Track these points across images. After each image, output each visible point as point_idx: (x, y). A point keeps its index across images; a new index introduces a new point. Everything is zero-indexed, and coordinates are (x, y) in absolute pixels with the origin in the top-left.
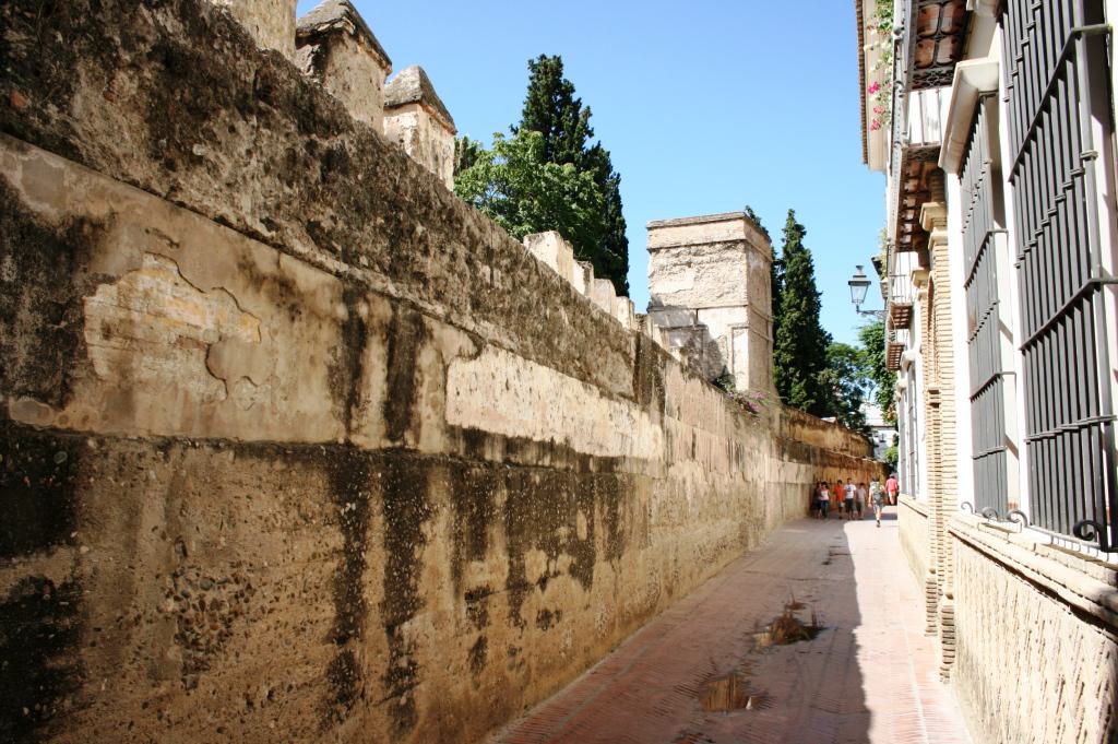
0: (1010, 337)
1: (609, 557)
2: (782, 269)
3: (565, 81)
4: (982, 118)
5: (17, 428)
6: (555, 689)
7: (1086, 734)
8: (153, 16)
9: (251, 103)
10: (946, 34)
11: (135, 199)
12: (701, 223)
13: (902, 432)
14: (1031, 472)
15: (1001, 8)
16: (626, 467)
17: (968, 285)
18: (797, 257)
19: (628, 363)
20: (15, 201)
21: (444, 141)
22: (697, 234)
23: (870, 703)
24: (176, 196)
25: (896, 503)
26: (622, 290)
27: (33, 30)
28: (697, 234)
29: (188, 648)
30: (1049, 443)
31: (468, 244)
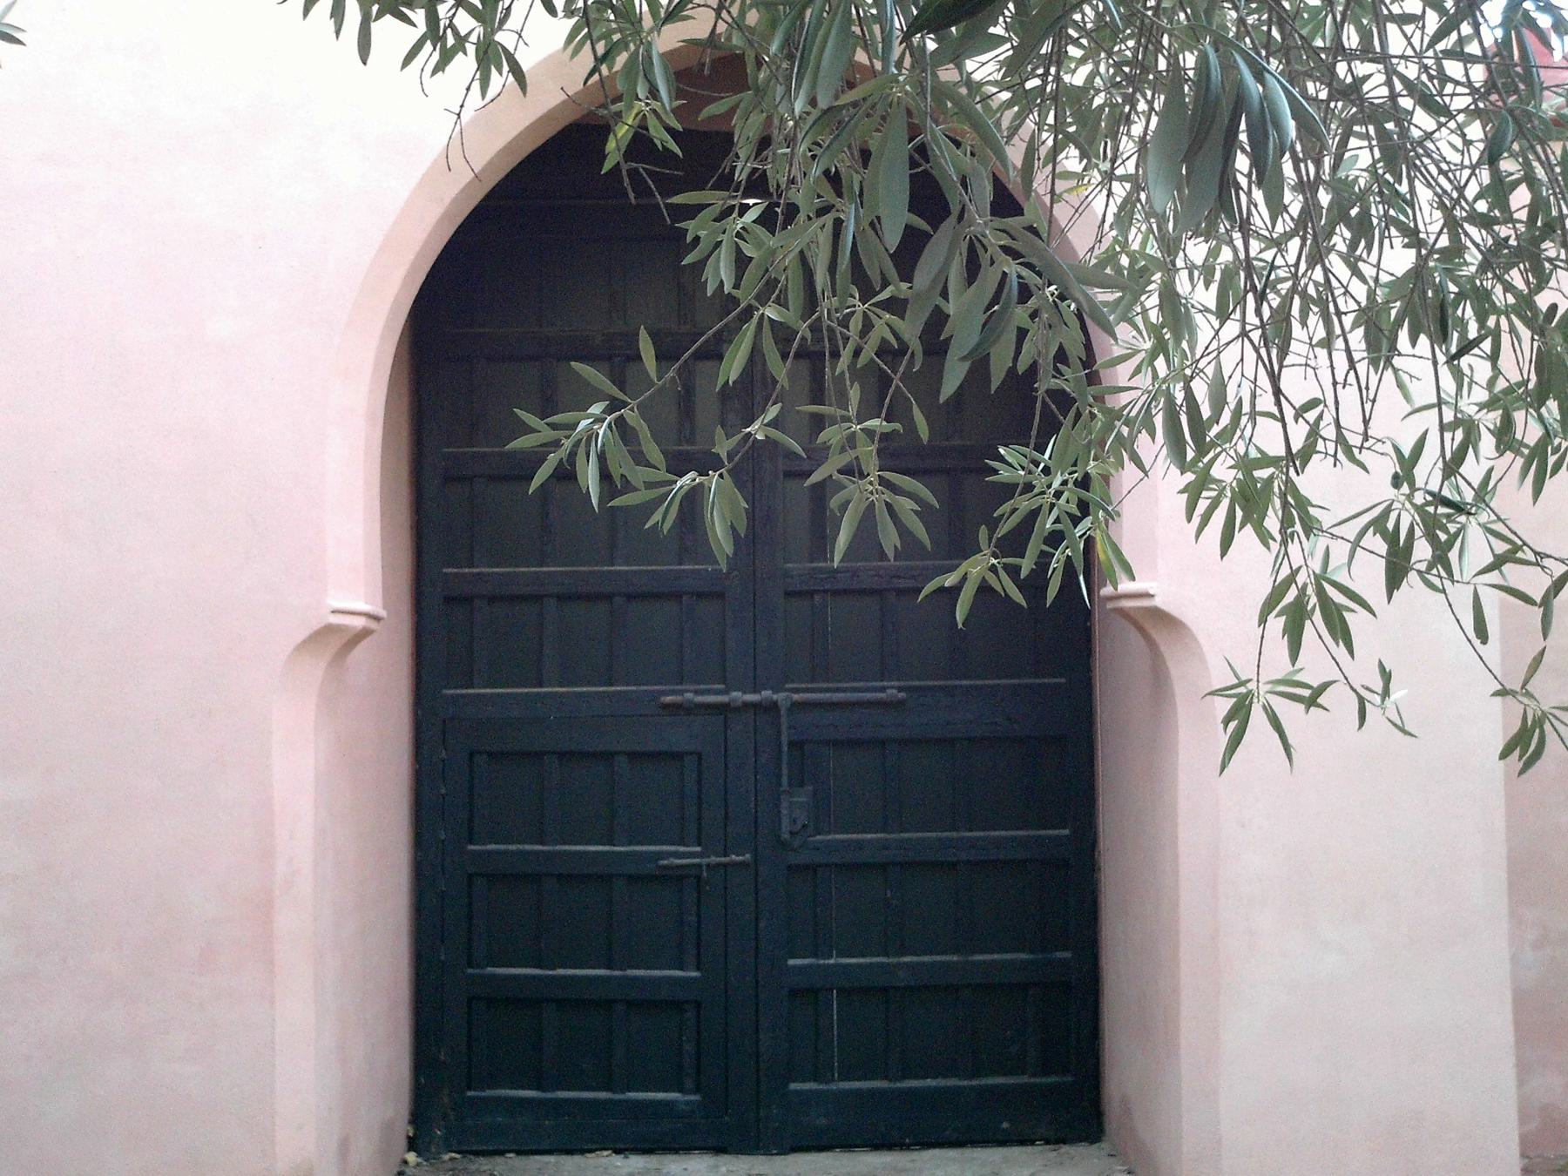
0: (1275, 540)
1: (704, 65)
2: (779, 207)
3: (1419, 137)
4: (671, 8)
5: (1092, 876)
6: (1216, 71)
7: (1367, 689)
8: (1014, 130)
9: (646, 44)
10: (1514, 226)
11: (964, 578)
12: (1399, 712)
13: (866, 109)
14: (1140, 591)
15: (356, 1175)
16: (763, 702)
17: (984, 326)
18: (818, 323)
19: (1278, 518)
20: (877, 533)
21: (819, 346)
22: (1069, 226)
23: (1514, 1070)
24: (1466, 264)
25: (470, 1001)
26: (848, 330)
27: (1297, 301)
28: (1069, 226)
29: (958, 860)
30: (1008, 50)
31: (1383, 71)
